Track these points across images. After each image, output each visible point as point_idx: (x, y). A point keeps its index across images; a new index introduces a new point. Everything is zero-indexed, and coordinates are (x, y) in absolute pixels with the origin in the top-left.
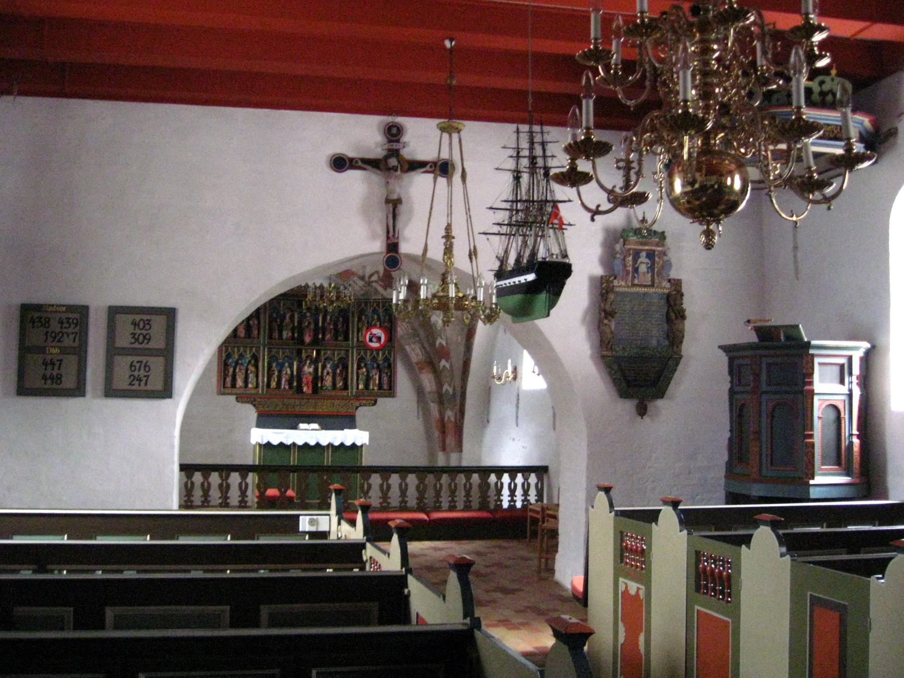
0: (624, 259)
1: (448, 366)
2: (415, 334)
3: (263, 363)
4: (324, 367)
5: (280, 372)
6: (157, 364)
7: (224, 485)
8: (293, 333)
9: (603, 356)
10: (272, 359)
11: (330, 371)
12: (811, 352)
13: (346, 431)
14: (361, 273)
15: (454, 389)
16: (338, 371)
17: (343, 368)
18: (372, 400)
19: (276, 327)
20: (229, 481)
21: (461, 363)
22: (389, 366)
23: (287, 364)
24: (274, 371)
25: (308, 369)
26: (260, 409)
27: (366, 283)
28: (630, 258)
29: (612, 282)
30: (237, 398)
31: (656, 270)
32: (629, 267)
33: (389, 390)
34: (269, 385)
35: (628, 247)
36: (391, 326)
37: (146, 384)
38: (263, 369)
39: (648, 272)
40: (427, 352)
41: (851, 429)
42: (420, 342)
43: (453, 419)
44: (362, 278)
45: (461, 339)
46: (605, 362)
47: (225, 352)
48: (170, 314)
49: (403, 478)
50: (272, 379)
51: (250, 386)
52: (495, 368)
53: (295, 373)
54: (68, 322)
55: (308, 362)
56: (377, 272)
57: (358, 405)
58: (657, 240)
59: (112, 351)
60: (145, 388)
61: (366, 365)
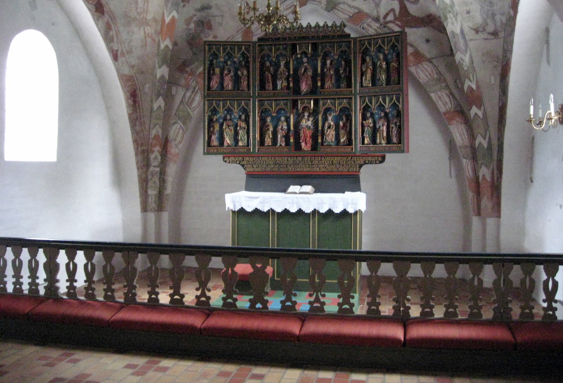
1: (480, 114)
2: (441, 79)
4: (325, 119)
5: (275, 128)
8: (289, 83)
10: (264, 113)
11: (332, 123)
13: (347, 193)
14: (375, 14)
16: (341, 124)
17: (347, 120)
18: (378, 157)
19: (270, 76)
21: (497, 108)
22: (399, 115)
23: (283, 118)
24: (268, 126)
25: (307, 123)
26: (248, 170)
27: (381, 25)
30: (224, 158)
34: (262, 142)
40: (456, 100)
42: (447, 87)
43: (488, 178)
44: (377, 20)
45: (495, 80)
51: (240, 144)
52: (532, 108)
55: (306, 114)
56: (393, 10)
57: (363, 163)
61: (372, 115)
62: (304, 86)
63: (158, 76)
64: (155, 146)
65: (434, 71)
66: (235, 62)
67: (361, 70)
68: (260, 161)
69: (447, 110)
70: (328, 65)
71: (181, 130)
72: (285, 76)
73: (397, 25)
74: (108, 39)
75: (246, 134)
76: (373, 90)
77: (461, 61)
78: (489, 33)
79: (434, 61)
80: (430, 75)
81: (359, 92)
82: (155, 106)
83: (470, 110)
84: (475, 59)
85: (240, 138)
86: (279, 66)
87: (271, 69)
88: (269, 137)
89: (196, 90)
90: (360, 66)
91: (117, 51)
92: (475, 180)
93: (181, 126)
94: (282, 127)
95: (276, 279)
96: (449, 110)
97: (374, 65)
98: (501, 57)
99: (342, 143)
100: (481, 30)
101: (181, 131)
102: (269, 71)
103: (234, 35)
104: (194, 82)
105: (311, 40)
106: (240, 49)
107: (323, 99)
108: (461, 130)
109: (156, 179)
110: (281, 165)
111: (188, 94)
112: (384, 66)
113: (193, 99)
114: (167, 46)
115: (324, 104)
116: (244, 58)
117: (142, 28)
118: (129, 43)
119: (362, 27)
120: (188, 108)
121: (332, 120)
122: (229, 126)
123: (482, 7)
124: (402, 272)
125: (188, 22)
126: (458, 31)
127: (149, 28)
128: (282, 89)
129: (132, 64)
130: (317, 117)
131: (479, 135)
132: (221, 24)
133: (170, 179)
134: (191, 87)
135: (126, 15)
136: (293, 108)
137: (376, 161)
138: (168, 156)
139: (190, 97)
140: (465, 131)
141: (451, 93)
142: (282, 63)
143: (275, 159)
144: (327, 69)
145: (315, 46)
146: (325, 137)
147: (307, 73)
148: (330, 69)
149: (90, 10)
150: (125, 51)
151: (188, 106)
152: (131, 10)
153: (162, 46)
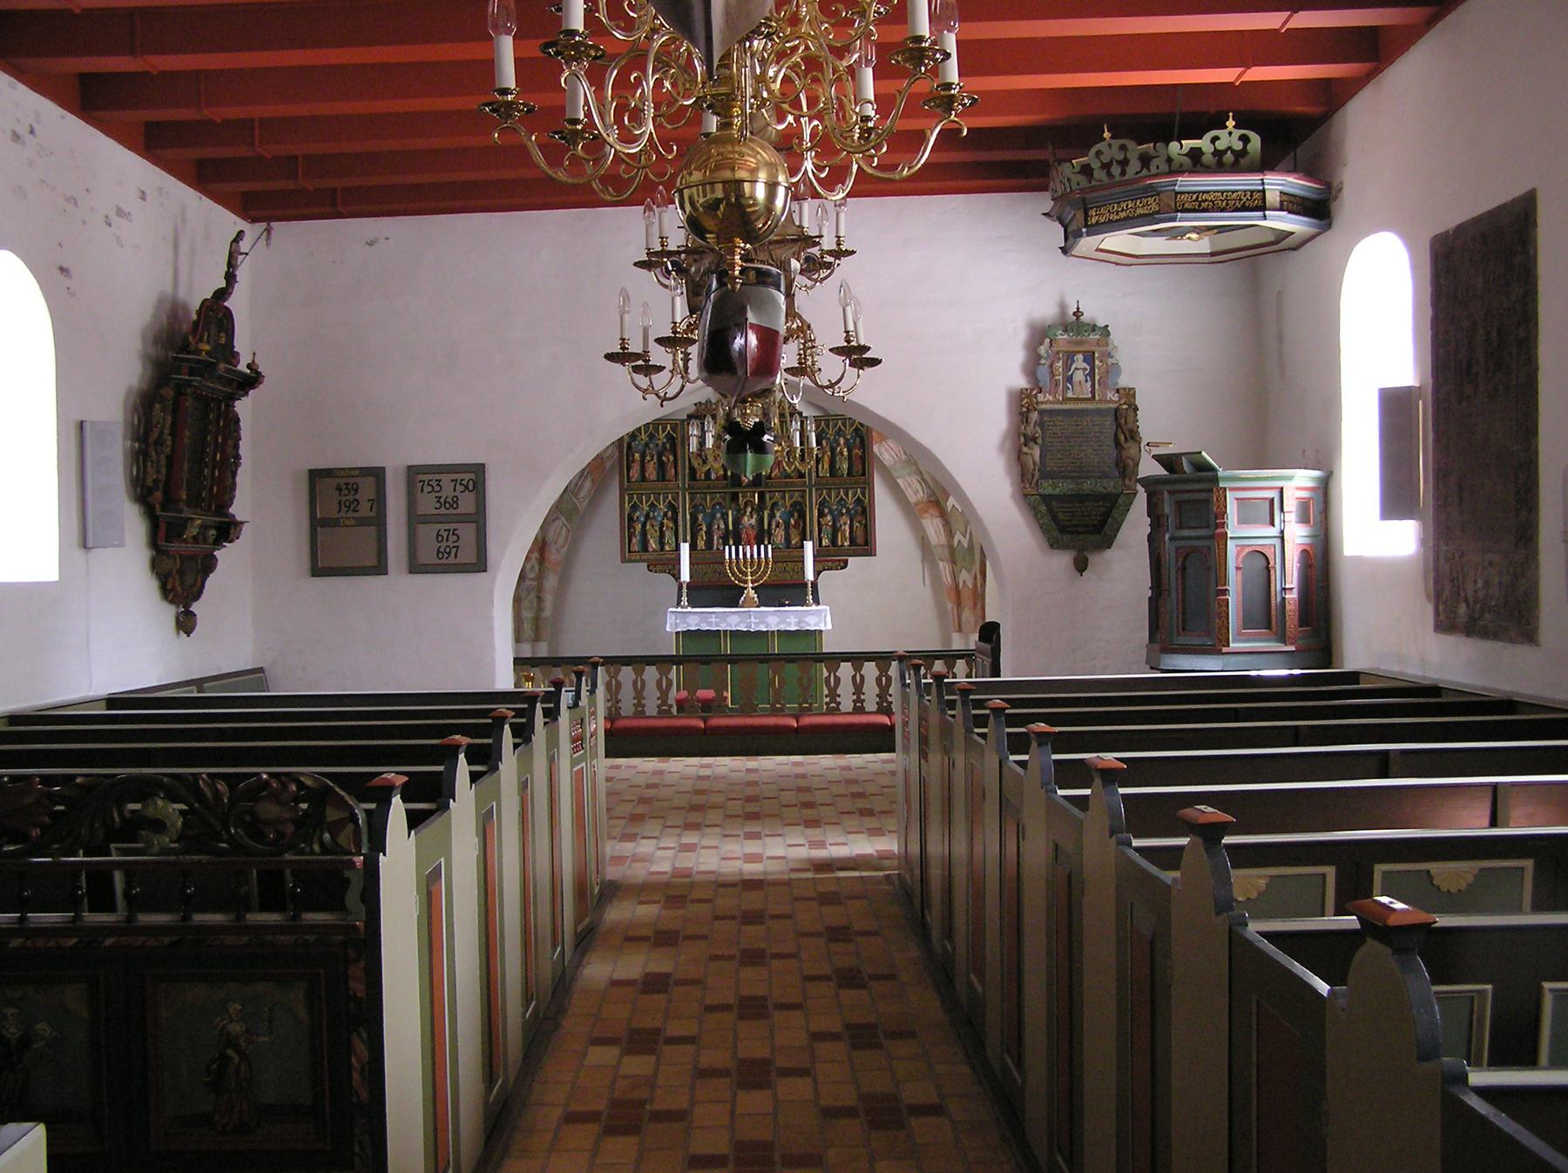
0: (1051, 366)
3: (685, 516)
4: (772, 516)
5: (709, 527)
6: (467, 532)
7: (614, 683)
9: (1025, 495)
12: (1221, 485)
15: (971, 541)
16: (792, 521)
17: (799, 516)
20: (620, 678)
22: (864, 511)
23: (719, 515)
28: (1060, 364)
29: (1036, 397)
30: (648, 567)
31: (1097, 378)
32: (1059, 375)
33: (864, 545)
35: (1055, 349)
36: (864, 452)
37: (456, 557)
38: (685, 526)
39: (1086, 381)
40: (928, 486)
41: (1290, 579)
43: (970, 585)
46: (1029, 504)
47: (629, 503)
48: (479, 470)
49: (857, 668)
50: (700, 538)
51: (667, 548)
53: (731, 528)
54: (347, 488)
57: (822, 569)
58: (1097, 337)
59: (415, 519)
60: (457, 561)
66: (657, 445)
69: (918, 499)
71: (564, 528)
76: (831, 481)
93: (563, 523)
94: (719, 527)
97: (833, 450)
106: (664, 430)
112: (846, 453)
120: (574, 499)
122: (653, 526)
131: (958, 532)
133: (549, 600)
140: (941, 526)
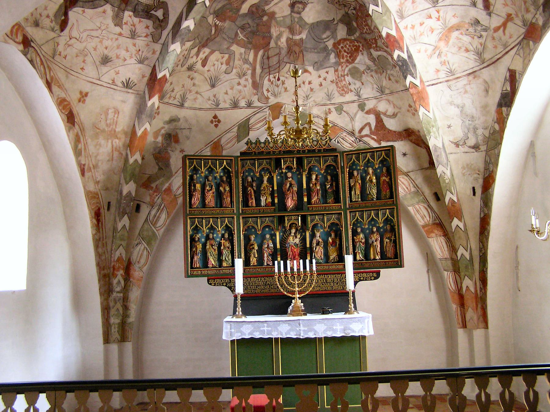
4: (313, 236)
5: (260, 246)
11: (320, 240)
14: (349, 128)
16: (330, 240)
21: (478, 220)
23: (268, 236)
24: (253, 244)
40: (434, 212)
44: (352, 133)
51: (225, 264)
55: (293, 231)
56: (369, 124)
62: (290, 202)
63: (125, 192)
64: (118, 271)
65: (411, 185)
66: (215, 178)
67: (350, 184)
68: (249, 282)
69: (425, 222)
70: (314, 180)
72: (269, 192)
73: (373, 139)
74: (78, 153)
75: (230, 254)
77: (443, 174)
78: (470, 147)
79: (409, 174)
80: (407, 188)
81: (349, 207)
82: (120, 226)
83: (451, 222)
84: (455, 173)
85: (224, 259)
86: (262, 182)
87: (254, 185)
88: (255, 256)
89: (162, 207)
90: (348, 181)
91: (84, 165)
92: (457, 292)
93: (145, 247)
94: (268, 246)
95: (326, 407)
96: (428, 223)
97: (363, 179)
98: (482, 170)
99: (332, 260)
100: (461, 143)
101: (145, 253)
102: (252, 186)
103: (202, 149)
104: (160, 199)
105: (296, 154)
107: (311, 215)
108: (440, 242)
109: (119, 306)
110: (272, 285)
111: (153, 212)
112: (374, 181)
113: (159, 217)
114: (136, 161)
115: (311, 221)
116: (224, 173)
117: (110, 141)
118: (96, 157)
119: (336, 141)
121: (319, 237)
122: (212, 246)
123: (463, 122)
124: (185, 398)
125: (156, 134)
126: (440, 145)
127: (117, 141)
128: (266, 205)
129: (98, 180)
130: (304, 234)
132: (188, 138)
134: (156, 204)
135: (95, 126)
136: (279, 224)
137: (371, 277)
138: (131, 280)
139: (155, 216)
141: (429, 206)
142: (265, 179)
143: (265, 279)
144: (313, 184)
145: (300, 162)
146: (314, 254)
147: (292, 188)
148: (316, 184)
149: (63, 120)
150: (91, 166)
151: (153, 225)
152: (100, 121)
153: (131, 161)
